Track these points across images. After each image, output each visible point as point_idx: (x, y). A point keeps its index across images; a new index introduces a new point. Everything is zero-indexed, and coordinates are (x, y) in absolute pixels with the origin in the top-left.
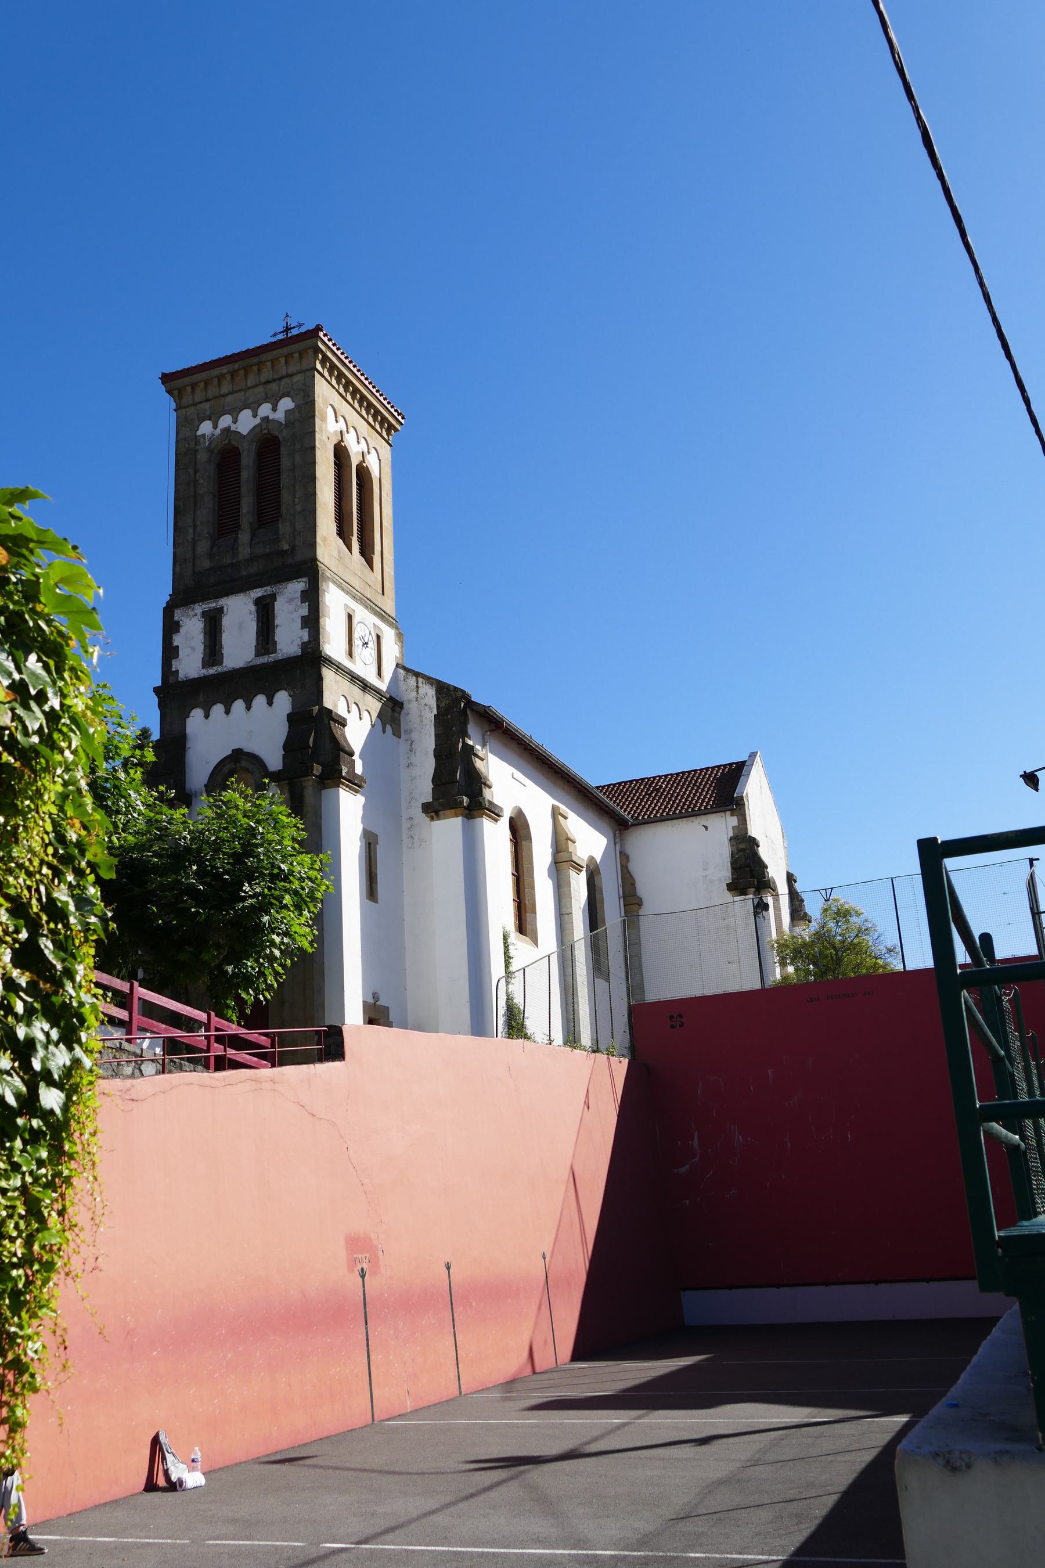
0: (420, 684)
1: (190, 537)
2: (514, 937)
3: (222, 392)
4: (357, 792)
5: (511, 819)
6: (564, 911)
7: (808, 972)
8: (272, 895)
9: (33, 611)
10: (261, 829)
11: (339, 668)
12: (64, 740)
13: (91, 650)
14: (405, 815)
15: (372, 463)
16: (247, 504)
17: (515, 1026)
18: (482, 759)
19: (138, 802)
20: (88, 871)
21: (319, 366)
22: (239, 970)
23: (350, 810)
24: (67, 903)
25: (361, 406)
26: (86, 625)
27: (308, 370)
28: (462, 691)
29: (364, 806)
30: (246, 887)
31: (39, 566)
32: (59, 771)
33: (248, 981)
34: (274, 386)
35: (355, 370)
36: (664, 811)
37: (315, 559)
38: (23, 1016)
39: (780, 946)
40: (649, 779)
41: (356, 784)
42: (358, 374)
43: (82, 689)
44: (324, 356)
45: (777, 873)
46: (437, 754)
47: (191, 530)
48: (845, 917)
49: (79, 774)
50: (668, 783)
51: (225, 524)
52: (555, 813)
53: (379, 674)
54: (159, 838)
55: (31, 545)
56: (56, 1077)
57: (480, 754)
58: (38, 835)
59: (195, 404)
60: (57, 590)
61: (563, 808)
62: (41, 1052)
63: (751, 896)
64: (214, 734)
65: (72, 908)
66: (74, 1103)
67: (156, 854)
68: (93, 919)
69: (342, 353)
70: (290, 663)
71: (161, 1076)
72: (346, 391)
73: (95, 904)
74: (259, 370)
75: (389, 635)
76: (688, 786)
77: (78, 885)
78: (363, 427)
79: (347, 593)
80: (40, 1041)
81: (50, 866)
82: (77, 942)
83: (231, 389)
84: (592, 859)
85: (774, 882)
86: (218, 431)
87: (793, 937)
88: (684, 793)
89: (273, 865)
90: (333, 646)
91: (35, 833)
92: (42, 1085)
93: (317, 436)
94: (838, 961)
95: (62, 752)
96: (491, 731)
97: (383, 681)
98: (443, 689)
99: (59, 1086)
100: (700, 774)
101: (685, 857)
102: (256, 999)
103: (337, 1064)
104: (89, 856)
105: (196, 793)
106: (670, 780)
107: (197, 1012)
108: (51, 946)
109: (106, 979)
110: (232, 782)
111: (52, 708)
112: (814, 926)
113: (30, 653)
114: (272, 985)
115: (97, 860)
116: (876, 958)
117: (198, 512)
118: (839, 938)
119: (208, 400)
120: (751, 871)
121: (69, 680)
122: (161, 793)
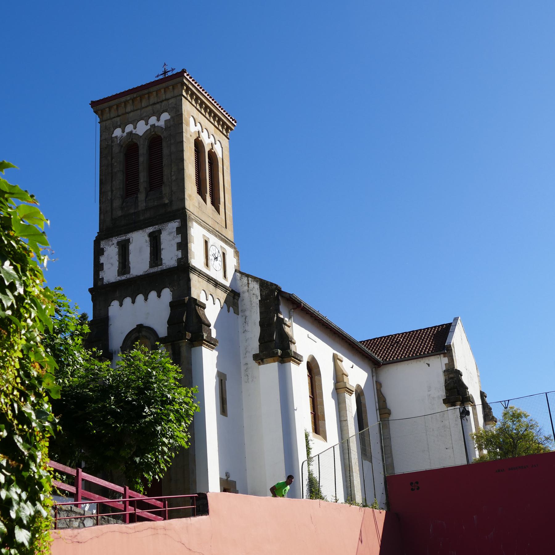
0: (250, 282)
1: (109, 198)
2: (312, 436)
3: (127, 111)
4: (213, 348)
5: (308, 363)
6: (343, 419)
7: (496, 454)
8: (162, 413)
9: (8, 236)
10: (154, 372)
11: (200, 273)
12: (27, 313)
13: (42, 258)
14: (243, 361)
15: (218, 149)
16: (143, 177)
17: (314, 491)
18: (289, 327)
19: (80, 358)
20: (44, 395)
21: (184, 93)
22: (144, 460)
23: (209, 360)
24: (30, 414)
25: (210, 116)
26: (39, 242)
27: (177, 96)
28: (275, 285)
29: (218, 357)
30: (147, 410)
31: (11, 208)
32: (23, 332)
33: (149, 467)
34: (158, 106)
35: (206, 95)
36: (402, 355)
37: (184, 208)
38: (4, 484)
39: (478, 437)
40: (392, 336)
41: (212, 343)
42: (208, 97)
43: (38, 281)
44: (187, 87)
45: (474, 391)
46: (262, 324)
47: (110, 193)
48: (518, 418)
49: (36, 333)
50: (404, 338)
51: (130, 189)
52: (335, 358)
53: (225, 276)
54: (93, 380)
55: (6, 196)
56: (25, 522)
57: (288, 323)
58: (11, 371)
59: (111, 119)
60: (21, 222)
61: (340, 355)
62: (16, 507)
63: (459, 407)
64: (125, 316)
65: (34, 417)
66: (37, 539)
67: (91, 390)
68: (47, 424)
69: (198, 85)
70: (170, 271)
71: (96, 527)
72: (201, 107)
73: (48, 415)
74: (149, 97)
75: (230, 252)
76: (417, 339)
77: (38, 403)
78: (212, 128)
79: (204, 228)
80: (15, 500)
81: (19, 390)
82: (38, 438)
83: (132, 109)
84: (358, 386)
85: (473, 398)
86: (125, 134)
87: (486, 432)
88: (414, 344)
89: (163, 395)
90: (197, 259)
91: (10, 370)
92: (17, 527)
93: (184, 134)
94: (515, 446)
95: (25, 321)
96: (294, 309)
97: (227, 281)
98: (264, 285)
99: (27, 528)
100: (423, 332)
101: (416, 384)
102: (154, 478)
103: (204, 517)
104: (44, 385)
105: (115, 351)
106: (405, 336)
107: (118, 487)
108: (21, 441)
109: (61, 467)
110: (137, 345)
111: (19, 293)
112: (499, 424)
113: (6, 260)
114: (164, 469)
115: (49, 387)
116: (539, 444)
117: (114, 182)
118: (514, 431)
119: (118, 116)
120: (458, 391)
121: (30, 277)
122: (94, 353)
